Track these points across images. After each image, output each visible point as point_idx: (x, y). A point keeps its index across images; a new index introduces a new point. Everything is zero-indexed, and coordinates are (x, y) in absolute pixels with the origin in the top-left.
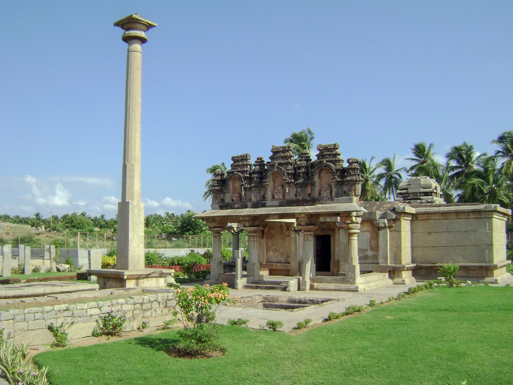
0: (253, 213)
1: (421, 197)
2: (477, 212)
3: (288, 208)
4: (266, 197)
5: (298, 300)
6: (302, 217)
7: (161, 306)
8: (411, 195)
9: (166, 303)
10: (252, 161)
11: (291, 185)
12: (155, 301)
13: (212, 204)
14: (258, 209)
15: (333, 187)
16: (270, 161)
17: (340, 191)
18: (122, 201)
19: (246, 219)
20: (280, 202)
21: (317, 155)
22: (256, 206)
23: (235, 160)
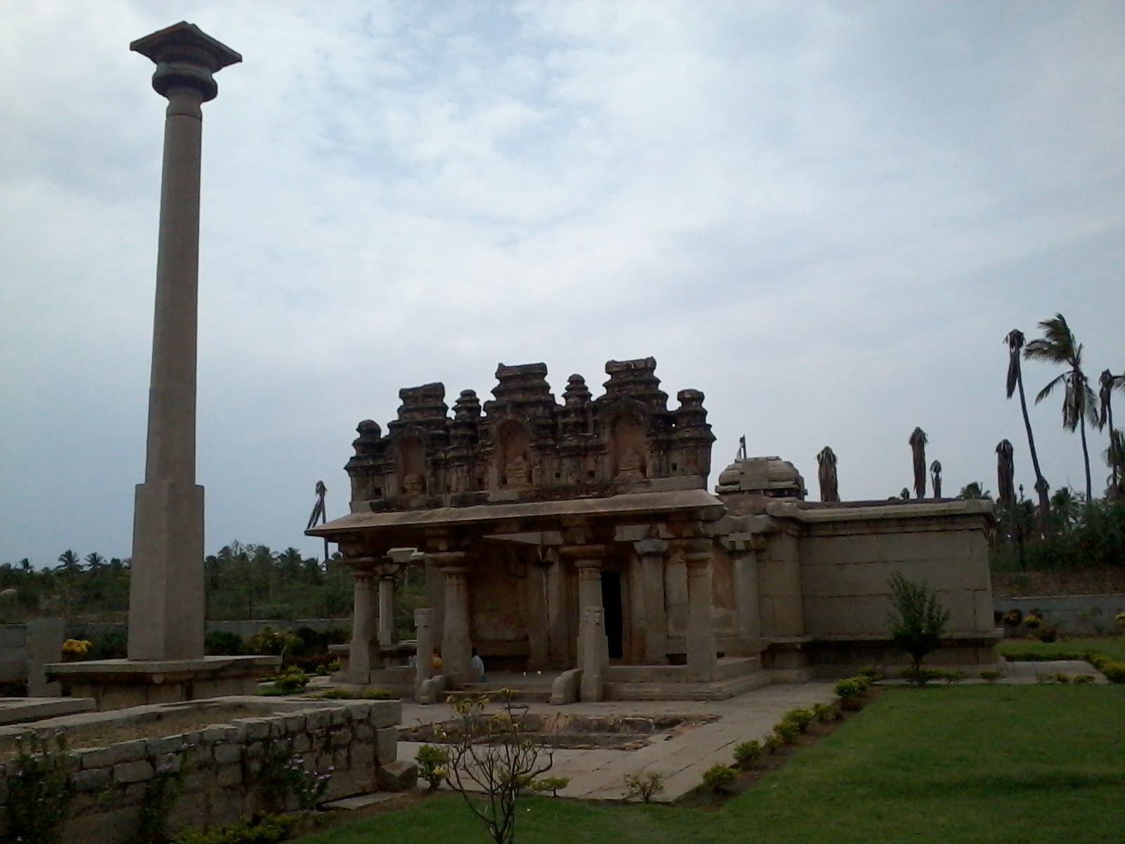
0: (459, 517)
2: (945, 517)
3: (543, 505)
4: (486, 480)
5: (596, 723)
6: (578, 526)
7: (316, 746)
9: (328, 737)
10: (451, 399)
11: (548, 453)
13: (352, 499)
17: (664, 463)
18: (400, 416)
19: (442, 532)
20: (523, 492)
21: (606, 385)
22: (463, 502)
23: (409, 397)
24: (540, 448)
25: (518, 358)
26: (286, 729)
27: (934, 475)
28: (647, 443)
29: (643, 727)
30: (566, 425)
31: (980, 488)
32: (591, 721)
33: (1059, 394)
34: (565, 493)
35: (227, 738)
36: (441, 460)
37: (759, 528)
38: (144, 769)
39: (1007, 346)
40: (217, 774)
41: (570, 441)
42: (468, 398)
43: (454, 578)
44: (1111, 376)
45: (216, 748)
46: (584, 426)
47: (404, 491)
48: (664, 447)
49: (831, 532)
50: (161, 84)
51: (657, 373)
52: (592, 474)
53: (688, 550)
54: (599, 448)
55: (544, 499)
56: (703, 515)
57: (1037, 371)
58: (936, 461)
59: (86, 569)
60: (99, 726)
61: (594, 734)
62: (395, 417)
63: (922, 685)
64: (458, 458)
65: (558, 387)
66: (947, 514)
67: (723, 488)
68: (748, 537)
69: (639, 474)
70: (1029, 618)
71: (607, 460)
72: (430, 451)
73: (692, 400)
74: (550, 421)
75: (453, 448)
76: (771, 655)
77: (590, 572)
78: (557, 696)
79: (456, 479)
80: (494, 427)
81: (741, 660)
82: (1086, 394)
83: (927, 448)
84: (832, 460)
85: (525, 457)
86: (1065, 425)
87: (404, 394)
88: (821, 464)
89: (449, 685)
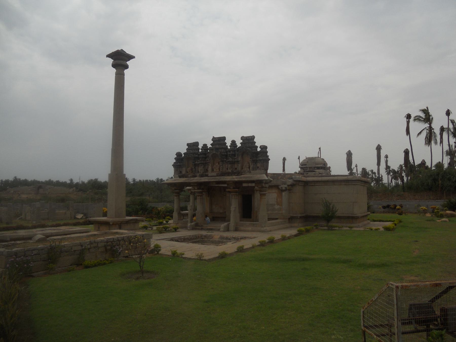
1: (315, 170)
2: (346, 181)
5: (226, 237)
8: (308, 169)
10: (200, 146)
12: (122, 240)
13: (174, 174)
14: (203, 178)
15: (251, 164)
16: (211, 147)
18: (187, 151)
19: (195, 184)
22: (202, 176)
24: (222, 161)
25: (218, 135)
26: (118, 239)
27: (386, 159)
28: (250, 161)
29: (242, 238)
30: (229, 154)
31: (411, 161)
32: (225, 237)
33: (424, 134)
34: (228, 174)
35: (102, 241)
36: (197, 164)
37: (289, 184)
38: (80, 248)
39: (405, 119)
40: (99, 249)
41: (230, 159)
42: (205, 146)
43: (199, 197)
44: (443, 127)
45: (98, 243)
46: (235, 155)
47: (187, 172)
48: (255, 162)
49: (314, 184)
50: (114, 66)
51: (255, 140)
52: (236, 169)
53: (260, 191)
54: (238, 162)
55: (223, 176)
56: (264, 182)
57: (416, 127)
58: (386, 155)
59: (132, 183)
60: (79, 237)
61: (225, 240)
62: (186, 151)
63: (332, 230)
64: (201, 163)
65: (228, 143)
66: (346, 180)
67: (302, 166)
68: (286, 186)
69: (248, 169)
70: (398, 207)
71: (240, 165)
72: (194, 161)
73: (264, 148)
74: (225, 153)
75: (200, 161)
76: (291, 219)
77: (234, 196)
78: (222, 230)
79: (201, 169)
80: (210, 155)
81: (281, 220)
82: (433, 134)
83: (382, 151)
84: (351, 154)
85: (219, 164)
86: (425, 144)
87: (188, 145)
88: (347, 155)
89: (197, 225)
